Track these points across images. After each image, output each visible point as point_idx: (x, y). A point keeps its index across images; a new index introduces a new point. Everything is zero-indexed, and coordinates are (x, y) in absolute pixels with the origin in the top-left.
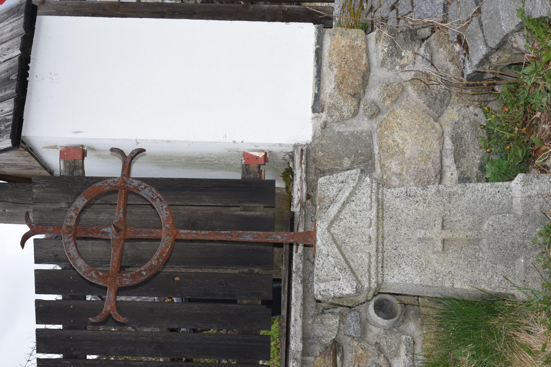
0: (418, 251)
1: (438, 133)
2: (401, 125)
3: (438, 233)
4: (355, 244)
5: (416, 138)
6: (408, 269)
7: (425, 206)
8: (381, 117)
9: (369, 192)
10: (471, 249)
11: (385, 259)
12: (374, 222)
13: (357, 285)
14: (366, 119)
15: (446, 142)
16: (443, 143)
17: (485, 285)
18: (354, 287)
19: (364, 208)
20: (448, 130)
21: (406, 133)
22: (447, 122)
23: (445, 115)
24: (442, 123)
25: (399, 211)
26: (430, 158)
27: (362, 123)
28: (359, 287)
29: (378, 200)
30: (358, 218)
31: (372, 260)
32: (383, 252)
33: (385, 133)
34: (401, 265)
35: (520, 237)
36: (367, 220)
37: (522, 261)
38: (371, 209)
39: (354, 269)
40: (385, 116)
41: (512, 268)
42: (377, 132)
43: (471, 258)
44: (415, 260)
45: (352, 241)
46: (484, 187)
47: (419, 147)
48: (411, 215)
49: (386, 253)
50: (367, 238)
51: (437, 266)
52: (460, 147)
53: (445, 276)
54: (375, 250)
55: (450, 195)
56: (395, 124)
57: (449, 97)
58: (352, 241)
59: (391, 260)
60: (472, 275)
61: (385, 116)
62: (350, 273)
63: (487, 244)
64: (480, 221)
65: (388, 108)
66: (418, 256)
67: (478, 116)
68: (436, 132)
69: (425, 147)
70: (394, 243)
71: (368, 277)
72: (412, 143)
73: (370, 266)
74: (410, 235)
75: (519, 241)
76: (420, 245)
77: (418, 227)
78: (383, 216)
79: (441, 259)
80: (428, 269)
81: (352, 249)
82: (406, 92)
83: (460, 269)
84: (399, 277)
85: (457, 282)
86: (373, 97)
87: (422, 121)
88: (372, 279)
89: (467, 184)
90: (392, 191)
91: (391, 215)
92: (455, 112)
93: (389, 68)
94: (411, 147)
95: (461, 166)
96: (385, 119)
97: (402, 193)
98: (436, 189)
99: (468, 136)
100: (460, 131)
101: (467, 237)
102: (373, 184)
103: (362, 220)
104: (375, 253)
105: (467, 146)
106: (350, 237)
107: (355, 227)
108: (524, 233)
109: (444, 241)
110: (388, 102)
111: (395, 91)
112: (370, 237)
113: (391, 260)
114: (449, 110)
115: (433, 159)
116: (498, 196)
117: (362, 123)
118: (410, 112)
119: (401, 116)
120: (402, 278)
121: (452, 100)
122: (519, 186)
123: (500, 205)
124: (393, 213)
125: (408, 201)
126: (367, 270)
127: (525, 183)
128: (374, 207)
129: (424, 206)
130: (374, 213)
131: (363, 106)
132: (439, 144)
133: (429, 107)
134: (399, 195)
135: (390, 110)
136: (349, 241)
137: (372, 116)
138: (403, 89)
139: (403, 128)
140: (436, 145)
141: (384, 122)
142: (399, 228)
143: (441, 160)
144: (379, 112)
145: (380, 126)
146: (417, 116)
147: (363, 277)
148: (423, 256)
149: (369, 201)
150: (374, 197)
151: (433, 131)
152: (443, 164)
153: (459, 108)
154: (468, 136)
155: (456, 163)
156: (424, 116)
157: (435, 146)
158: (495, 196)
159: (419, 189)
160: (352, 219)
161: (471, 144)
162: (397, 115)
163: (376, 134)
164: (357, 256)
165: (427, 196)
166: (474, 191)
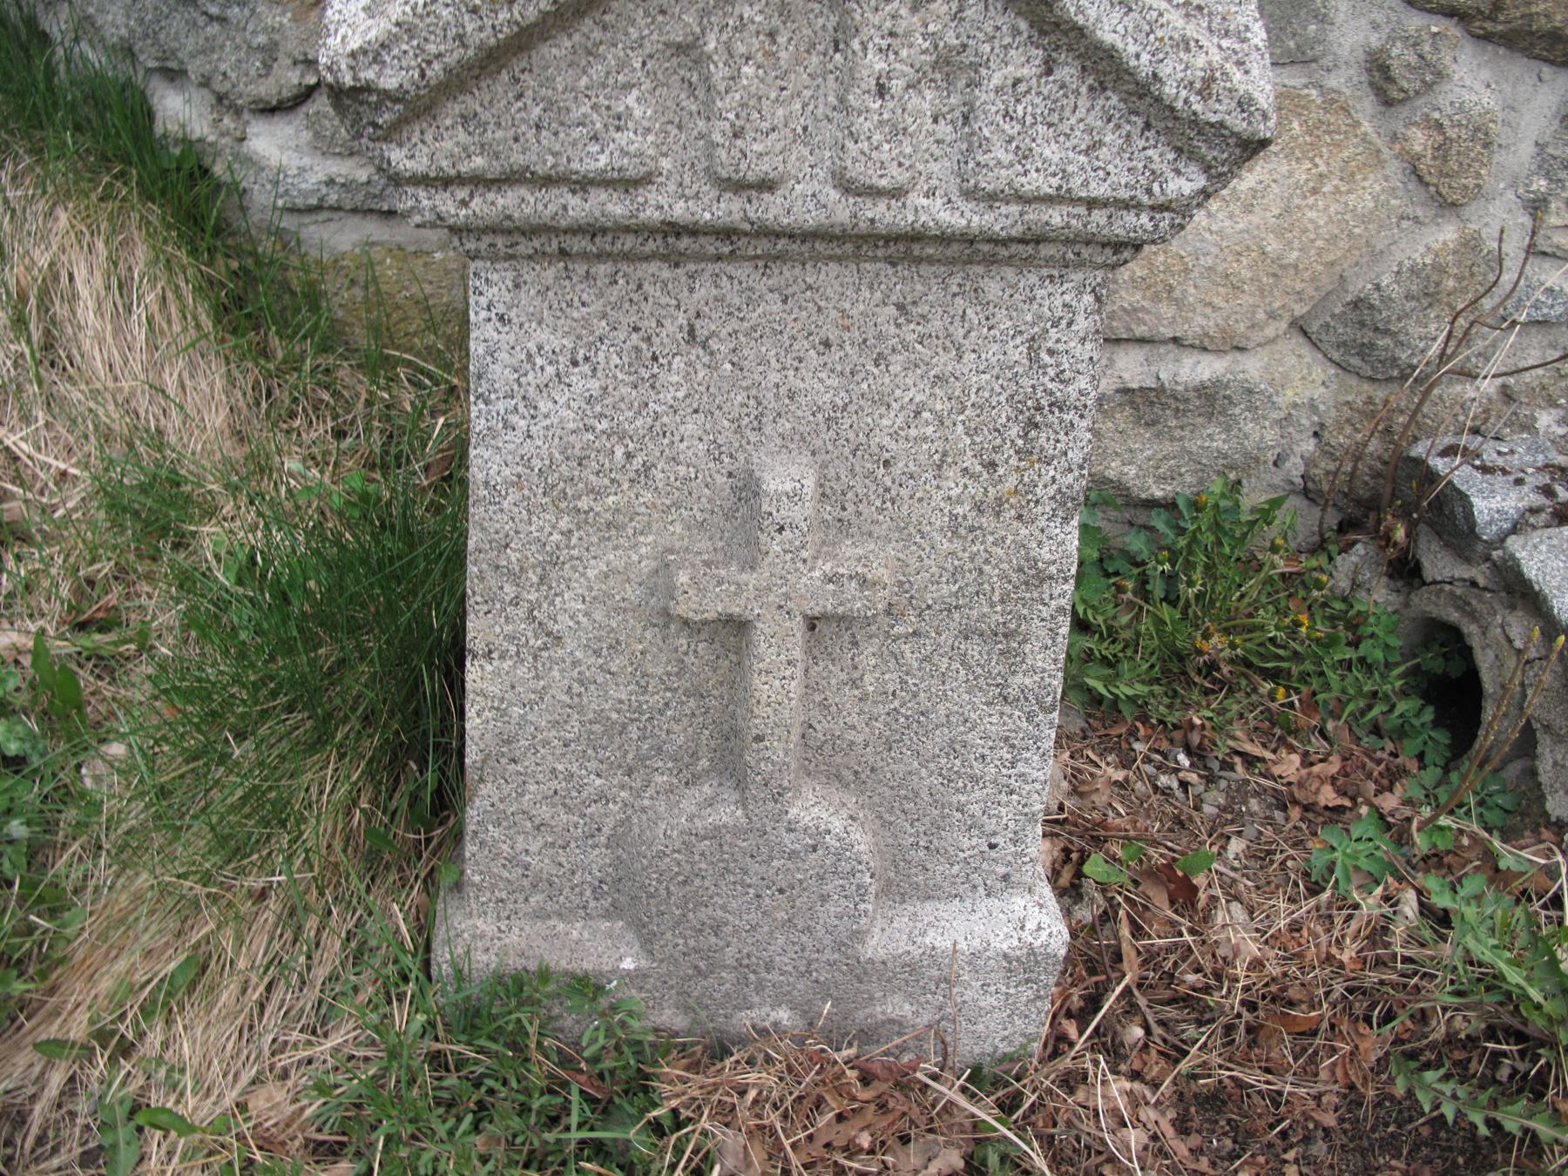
0: (682, 470)
1: (1249, 333)
2: (1314, 191)
3: (787, 597)
4: (719, 73)
5: (1248, 248)
6: (561, 409)
7: (959, 510)
8: (1365, 106)
9: (1099, 190)
10: (696, 739)
11: (624, 267)
12: (882, 213)
13: (386, 95)
14: (1375, 41)
15: (1206, 359)
16: (1205, 349)
17: (495, 799)
18: (369, 74)
19: (985, 145)
20: (1252, 367)
21: (1276, 212)
22: (1280, 362)
23: (1306, 351)
24: (1281, 346)
25: (944, 362)
26: (1156, 299)
27: (1363, 22)
28: (377, 107)
29: (1035, 238)
30: (914, 101)
31: (599, 196)
32: (675, 260)
33: (1295, 125)
34: (586, 368)
35: (748, 956)
36: (894, 170)
37: (628, 964)
38: (970, 194)
39: (518, 64)
40: (1366, 127)
41: (592, 904)
42: (1306, 86)
43: (641, 739)
44: (619, 452)
45: (741, 48)
46: (1028, 787)
47: (1210, 261)
48: (913, 432)
49: (666, 274)
50: (764, 168)
51: (591, 573)
52: (1177, 410)
53: (531, 617)
54: (679, 211)
55: (1005, 636)
56: (1323, 168)
57: (1370, 373)
58: (741, 48)
59: (616, 306)
60: (545, 743)
61: (1366, 127)
62: (475, 39)
63: (717, 828)
64: (845, 772)
65: (1394, 137)
66: (647, 468)
67: (1273, 469)
68: (1253, 326)
69: (1200, 283)
70: (734, 324)
71: (464, 168)
72: (1230, 231)
73: (548, 181)
74: (786, 426)
75: (730, 952)
76: (721, 480)
77: (831, 473)
78: (919, 261)
79: (632, 593)
80: (564, 523)
81: (681, 49)
82: (1436, 216)
83: (576, 688)
84: (503, 356)
85: (497, 673)
86: (1456, 77)
87: (1306, 275)
88: (462, 193)
89: (1056, 714)
90: (1080, 318)
91: (923, 309)
92: (1308, 394)
93: (1550, 150)
94: (1214, 228)
95: (1105, 412)
96: (1357, 124)
97: (1059, 377)
98: (1053, 569)
99: (1213, 440)
100: (1237, 411)
101: (759, 738)
102: (1144, 219)
103: (897, 132)
104: (651, 215)
105: (1178, 433)
106: (772, 35)
107: (847, 79)
108: (769, 967)
109: (736, 628)
110: (1419, 140)
111: (1456, 175)
112: (767, 185)
113: (616, 306)
114: (1321, 371)
115: (1148, 312)
116: (971, 843)
117: (1363, 22)
118: (1357, 231)
119: (1349, 192)
120: (501, 374)
121: (1353, 381)
122: (1008, 936)
123: (921, 853)
124: (936, 325)
125: (1007, 411)
126: (518, 159)
127: (1021, 965)
128: (989, 217)
129: (959, 501)
130: (945, 217)
131: (1434, 29)
132: (1206, 334)
133: (1356, 304)
134: (1046, 358)
135: (1385, 150)
136: (742, 24)
137: (1378, 71)
138: (1447, 206)
139: (1297, 201)
140: (1198, 323)
141: (1341, 121)
142: (836, 354)
143: (1141, 341)
144: (1388, 103)
145: (1332, 101)
146: (1331, 257)
147: (462, 136)
148: (648, 496)
149: (1036, 182)
150: (1056, 217)
151: (1261, 315)
152: (1124, 346)
153: (1322, 408)
154: (1213, 440)
155: (1117, 391)
156: (1324, 280)
157: (1200, 320)
158: (975, 832)
159: (1070, 478)
160: (916, 50)
161: (1183, 448)
162: (1359, 177)
163: (1298, 82)
164: (628, 87)
165: (1020, 517)
166: (1013, 746)
